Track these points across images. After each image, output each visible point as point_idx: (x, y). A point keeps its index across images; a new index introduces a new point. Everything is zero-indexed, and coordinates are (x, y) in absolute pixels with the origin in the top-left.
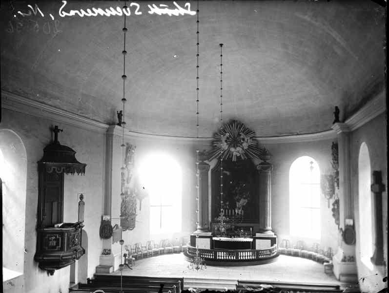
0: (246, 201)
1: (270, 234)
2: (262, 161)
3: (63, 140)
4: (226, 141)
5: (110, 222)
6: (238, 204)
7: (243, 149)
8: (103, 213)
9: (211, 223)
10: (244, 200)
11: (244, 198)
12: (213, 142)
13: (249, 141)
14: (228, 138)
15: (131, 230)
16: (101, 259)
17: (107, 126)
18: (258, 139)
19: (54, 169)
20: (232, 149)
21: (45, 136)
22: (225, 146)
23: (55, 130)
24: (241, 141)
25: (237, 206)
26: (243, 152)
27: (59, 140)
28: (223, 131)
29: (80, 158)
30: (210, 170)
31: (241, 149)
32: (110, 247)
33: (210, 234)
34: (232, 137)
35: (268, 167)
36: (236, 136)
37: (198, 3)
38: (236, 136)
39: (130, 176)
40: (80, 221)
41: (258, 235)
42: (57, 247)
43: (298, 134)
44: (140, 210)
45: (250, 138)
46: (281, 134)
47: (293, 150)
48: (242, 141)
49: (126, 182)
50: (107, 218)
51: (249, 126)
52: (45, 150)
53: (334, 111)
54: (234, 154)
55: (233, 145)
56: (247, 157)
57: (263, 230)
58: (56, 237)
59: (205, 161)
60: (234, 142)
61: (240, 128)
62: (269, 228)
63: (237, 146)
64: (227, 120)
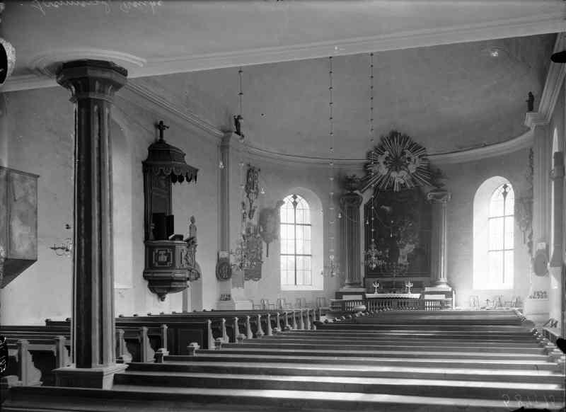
0: (413, 246)
1: (443, 287)
2: (436, 188)
3: (169, 139)
4: (385, 163)
5: (229, 260)
6: (402, 252)
7: (409, 172)
8: (220, 248)
9: (364, 279)
10: (411, 246)
11: (410, 243)
12: (366, 166)
13: (417, 161)
14: (387, 158)
15: (256, 280)
16: (218, 304)
17: (223, 134)
18: (428, 157)
19: (162, 170)
20: (394, 174)
21: (150, 136)
22: (383, 170)
23: (160, 126)
24: (405, 162)
25: (401, 254)
26: (409, 177)
27: (164, 139)
28: (380, 149)
29: (190, 161)
30: (362, 209)
31: (406, 173)
32: (230, 291)
33: (362, 290)
34: (394, 157)
35: (443, 195)
36: (399, 155)
37: (512, 216)
38: (399, 155)
39: (253, 208)
40: (192, 235)
41: (427, 289)
42: (168, 263)
43: (485, 146)
44: (267, 256)
45: (419, 157)
46: (461, 148)
47: (482, 170)
48: (407, 162)
49: (247, 216)
50: (224, 255)
51: (418, 141)
52: (150, 149)
53: (528, 98)
54: (396, 181)
55: (394, 167)
56: (415, 183)
57: (434, 283)
58: (166, 251)
59: (355, 192)
60: (396, 163)
61: (405, 143)
62: (443, 280)
63: (401, 169)
64: (387, 133)
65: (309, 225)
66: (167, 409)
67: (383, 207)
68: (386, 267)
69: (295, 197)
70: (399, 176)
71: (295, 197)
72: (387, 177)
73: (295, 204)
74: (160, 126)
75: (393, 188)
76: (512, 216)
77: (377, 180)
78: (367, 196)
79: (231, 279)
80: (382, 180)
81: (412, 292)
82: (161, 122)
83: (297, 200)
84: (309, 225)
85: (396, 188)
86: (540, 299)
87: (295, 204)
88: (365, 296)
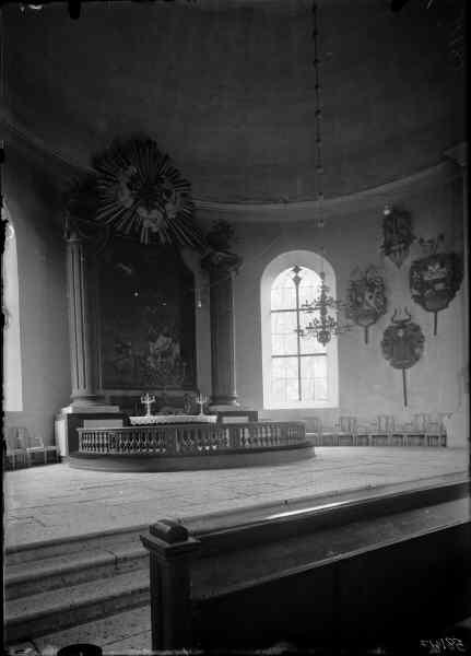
7: (165, 215)
10: (165, 339)
13: (178, 201)
20: (142, 212)
22: (126, 198)
24: (161, 197)
48: (165, 197)
54: (145, 224)
63: (154, 207)
65: (324, 354)
69: (297, 270)
70: (150, 217)
71: (297, 270)
73: (297, 280)
76: (404, 372)
77: (114, 214)
80: (121, 215)
81: (153, 413)
83: (300, 274)
84: (324, 354)
85: (145, 239)
87: (297, 280)
88: (129, 420)
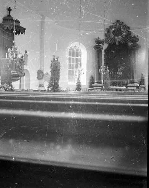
20: (116, 37)
21: (6, 14)
54: (117, 40)
66: (58, 147)
67: (112, 51)
68: (56, 79)
72: (113, 39)
74: (9, 10)
75: (116, 43)
78: (105, 46)
79: (44, 78)
82: (10, 8)
86: (42, 84)
